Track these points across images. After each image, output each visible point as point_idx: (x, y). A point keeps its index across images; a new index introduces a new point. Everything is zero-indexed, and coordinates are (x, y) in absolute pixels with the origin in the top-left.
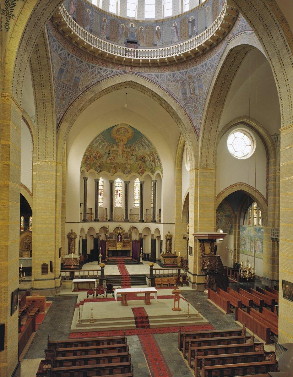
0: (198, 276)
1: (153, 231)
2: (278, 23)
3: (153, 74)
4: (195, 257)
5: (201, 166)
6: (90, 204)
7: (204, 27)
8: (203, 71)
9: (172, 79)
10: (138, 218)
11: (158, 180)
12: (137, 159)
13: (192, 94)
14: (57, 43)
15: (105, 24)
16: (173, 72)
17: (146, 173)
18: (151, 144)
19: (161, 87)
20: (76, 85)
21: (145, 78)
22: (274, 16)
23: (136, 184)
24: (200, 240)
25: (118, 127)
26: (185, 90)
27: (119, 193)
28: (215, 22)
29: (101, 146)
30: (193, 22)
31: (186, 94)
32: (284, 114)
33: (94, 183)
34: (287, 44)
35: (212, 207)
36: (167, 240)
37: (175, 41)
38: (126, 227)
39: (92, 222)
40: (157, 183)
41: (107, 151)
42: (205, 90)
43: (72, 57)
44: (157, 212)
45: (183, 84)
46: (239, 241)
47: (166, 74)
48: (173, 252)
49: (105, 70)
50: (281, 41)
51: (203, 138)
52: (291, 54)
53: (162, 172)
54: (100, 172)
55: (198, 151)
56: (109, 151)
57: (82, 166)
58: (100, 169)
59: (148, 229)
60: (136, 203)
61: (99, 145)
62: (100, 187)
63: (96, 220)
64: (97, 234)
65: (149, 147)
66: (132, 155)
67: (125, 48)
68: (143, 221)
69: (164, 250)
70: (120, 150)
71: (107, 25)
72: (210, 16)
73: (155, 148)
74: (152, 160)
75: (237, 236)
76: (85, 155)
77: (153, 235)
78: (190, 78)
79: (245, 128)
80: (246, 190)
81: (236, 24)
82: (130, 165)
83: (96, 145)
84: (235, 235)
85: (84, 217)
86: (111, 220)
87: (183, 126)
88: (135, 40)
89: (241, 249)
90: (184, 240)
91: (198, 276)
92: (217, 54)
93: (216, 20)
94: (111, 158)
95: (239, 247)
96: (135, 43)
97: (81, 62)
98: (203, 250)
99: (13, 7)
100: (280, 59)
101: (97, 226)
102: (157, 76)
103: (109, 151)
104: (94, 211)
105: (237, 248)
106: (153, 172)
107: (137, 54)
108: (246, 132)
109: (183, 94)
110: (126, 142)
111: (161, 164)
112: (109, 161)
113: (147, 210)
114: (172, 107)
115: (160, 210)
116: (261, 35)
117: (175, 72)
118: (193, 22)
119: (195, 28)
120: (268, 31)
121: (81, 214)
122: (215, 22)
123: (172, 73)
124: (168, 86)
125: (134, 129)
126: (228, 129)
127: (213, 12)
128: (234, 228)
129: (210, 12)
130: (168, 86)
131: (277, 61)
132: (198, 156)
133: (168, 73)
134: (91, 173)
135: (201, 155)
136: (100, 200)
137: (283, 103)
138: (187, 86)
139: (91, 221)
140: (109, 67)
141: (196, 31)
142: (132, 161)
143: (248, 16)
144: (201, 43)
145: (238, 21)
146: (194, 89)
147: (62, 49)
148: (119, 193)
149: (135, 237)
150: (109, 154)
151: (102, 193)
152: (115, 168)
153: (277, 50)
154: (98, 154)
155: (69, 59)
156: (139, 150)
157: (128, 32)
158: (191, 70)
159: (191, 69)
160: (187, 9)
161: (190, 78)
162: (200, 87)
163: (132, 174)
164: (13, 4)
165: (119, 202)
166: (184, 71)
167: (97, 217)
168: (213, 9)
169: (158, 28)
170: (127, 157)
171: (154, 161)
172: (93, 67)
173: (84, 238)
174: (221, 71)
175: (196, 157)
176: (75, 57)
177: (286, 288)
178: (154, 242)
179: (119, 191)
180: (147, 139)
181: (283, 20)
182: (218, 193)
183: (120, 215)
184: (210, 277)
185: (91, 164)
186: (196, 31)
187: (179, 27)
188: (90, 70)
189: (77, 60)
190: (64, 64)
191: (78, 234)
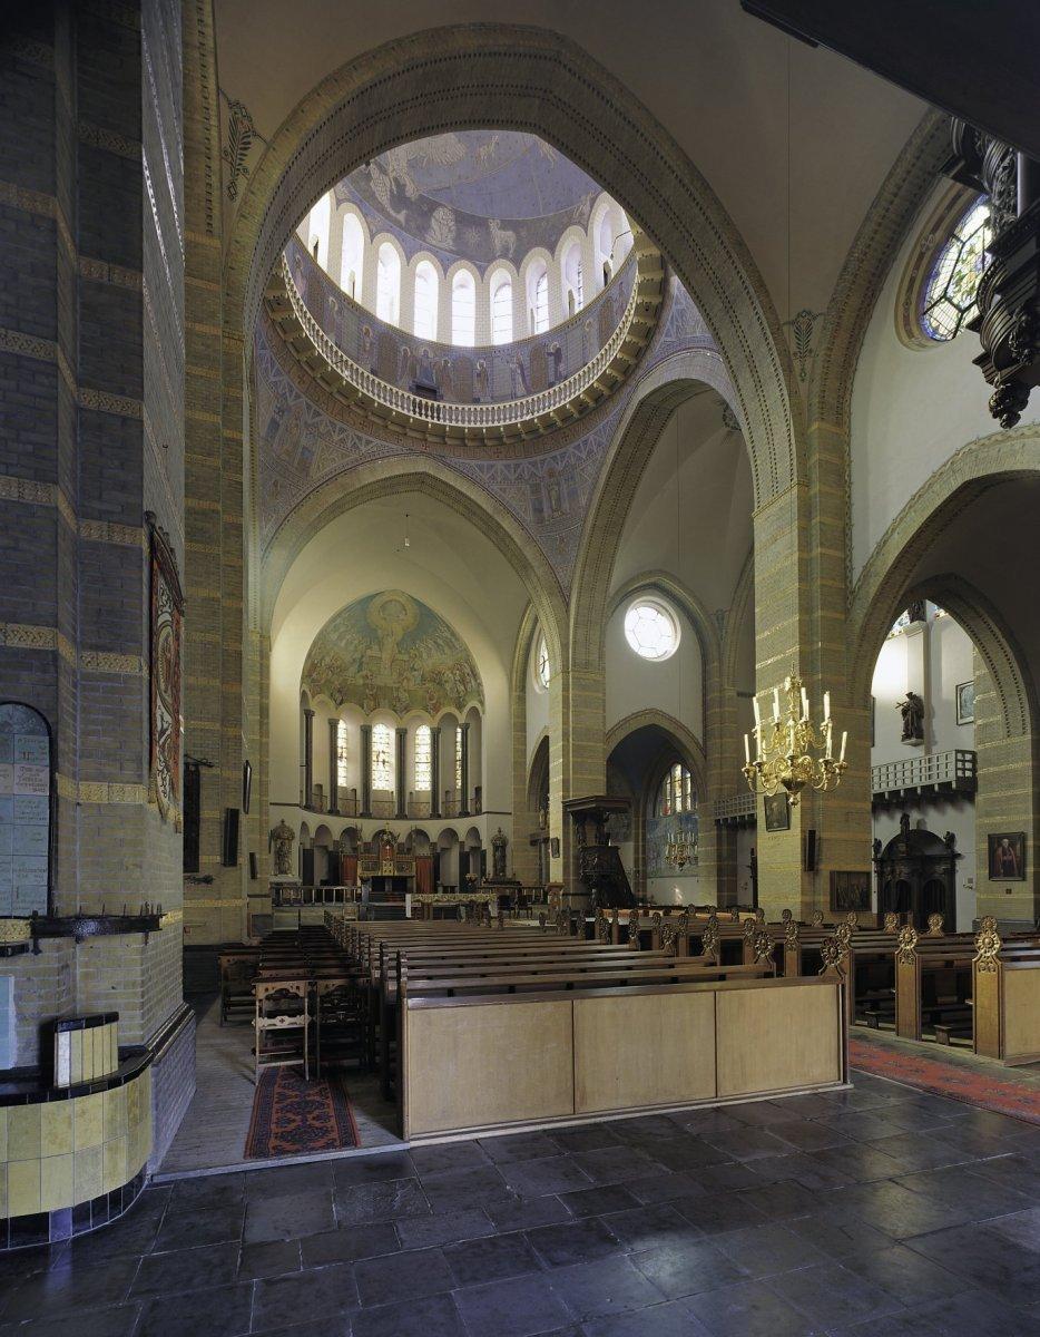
0: (573, 895)
1: (462, 836)
2: (752, 290)
3: (473, 463)
4: (566, 857)
5: (574, 666)
6: (319, 775)
7: (581, 364)
8: (580, 459)
9: (513, 477)
10: (427, 810)
11: (472, 726)
12: (423, 679)
13: (553, 511)
14: (268, 353)
15: (367, 340)
16: (515, 462)
17: (444, 710)
18: (457, 639)
19: (489, 493)
20: (305, 468)
21: (456, 470)
22: (745, 276)
23: (420, 737)
24: (574, 813)
25: (385, 598)
26: (541, 503)
27: (382, 757)
28: (603, 352)
29: (343, 644)
30: (558, 355)
31: (541, 511)
32: (779, 402)
33: (326, 727)
34: (769, 333)
35: (600, 752)
36: (496, 848)
37: (519, 394)
38: (401, 829)
39: (325, 814)
40: (469, 731)
41: (357, 656)
42: (583, 501)
43: (297, 397)
44: (471, 794)
45: (536, 489)
46: (644, 852)
47: (500, 465)
48: (509, 875)
49: (368, 442)
50: (757, 328)
51: (578, 606)
52: (776, 354)
53: (482, 703)
54: (340, 704)
55: (568, 635)
56: (362, 656)
57: (302, 683)
58: (344, 696)
59: (450, 834)
60: (422, 781)
61: (340, 638)
62: (341, 743)
63: (333, 812)
64: (336, 843)
65: (452, 647)
66: (413, 669)
67: (412, 397)
68: (439, 817)
69: (490, 868)
70: (386, 656)
71: (371, 344)
72: (594, 340)
73: (466, 650)
74: (458, 678)
75: (641, 844)
76: (309, 656)
77: (462, 844)
78: (551, 474)
79: (659, 597)
80: (665, 725)
81: (652, 345)
82: (409, 691)
83: (334, 636)
84: (637, 841)
85: (307, 799)
86: (366, 815)
87: (535, 580)
88: (433, 384)
89: (649, 869)
90: (532, 852)
91: (573, 895)
92: (610, 417)
93: (607, 347)
94: (364, 673)
95: (645, 864)
96: (435, 392)
97: (317, 414)
98: (582, 839)
99: (246, 149)
100: (753, 370)
101: (337, 825)
102: (481, 468)
103: (362, 656)
104: (327, 790)
105: (641, 868)
106: (460, 707)
107: (438, 414)
108: (659, 604)
109: (535, 510)
110: (399, 638)
111: (480, 684)
112: (361, 682)
113: (447, 792)
114: (513, 536)
115: (478, 790)
116: (717, 325)
117: (521, 461)
118: (558, 355)
119: (562, 367)
120: (731, 312)
121: (301, 792)
122: (603, 352)
123: (512, 462)
124: (505, 492)
125: (421, 605)
126: (622, 601)
127: (601, 331)
128: (633, 826)
129: (594, 331)
130: (505, 492)
131: (748, 375)
132: (568, 643)
133: (504, 462)
134: (322, 702)
135: (575, 642)
136: (341, 772)
137: (758, 462)
138: (544, 492)
139: (321, 812)
140: (378, 437)
141: (564, 373)
142: (411, 684)
143: (693, 283)
144: (577, 393)
145: (657, 337)
146: (559, 500)
147: (278, 373)
148: (382, 757)
149: (425, 851)
150: (361, 664)
151: (344, 755)
152: (375, 697)
153: (747, 353)
154: (336, 660)
155: (291, 402)
156: (429, 656)
157: (418, 367)
158: (554, 458)
159: (553, 454)
160: (543, 327)
161: (551, 474)
162: (573, 494)
163: (413, 713)
164: (244, 143)
165: (383, 780)
166: (538, 458)
167: (334, 804)
168: (601, 326)
169: (481, 365)
170: (400, 674)
171: (463, 681)
172: (342, 430)
173: (308, 847)
174: (618, 453)
175: (565, 646)
176: (304, 399)
177: (772, 809)
178: (464, 859)
179: (381, 755)
180: (448, 627)
181: (761, 285)
182: (609, 727)
183: (386, 805)
184: (599, 893)
185: (322, 682)
186: (564, 373)
187: (527, 364)
188: (336, 438)
189: (309, 407)
190: (281, 411)
191: (297, 830)
